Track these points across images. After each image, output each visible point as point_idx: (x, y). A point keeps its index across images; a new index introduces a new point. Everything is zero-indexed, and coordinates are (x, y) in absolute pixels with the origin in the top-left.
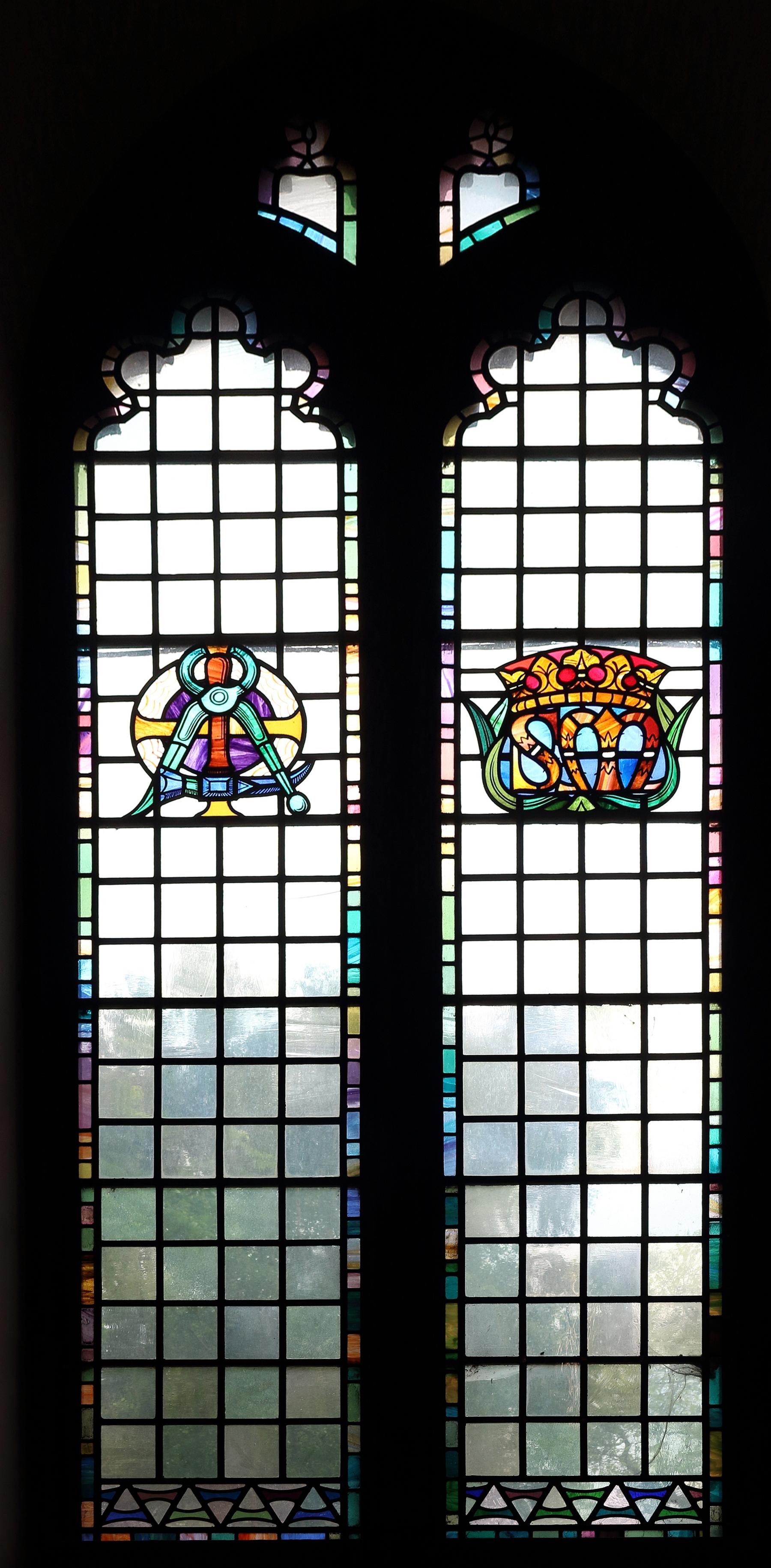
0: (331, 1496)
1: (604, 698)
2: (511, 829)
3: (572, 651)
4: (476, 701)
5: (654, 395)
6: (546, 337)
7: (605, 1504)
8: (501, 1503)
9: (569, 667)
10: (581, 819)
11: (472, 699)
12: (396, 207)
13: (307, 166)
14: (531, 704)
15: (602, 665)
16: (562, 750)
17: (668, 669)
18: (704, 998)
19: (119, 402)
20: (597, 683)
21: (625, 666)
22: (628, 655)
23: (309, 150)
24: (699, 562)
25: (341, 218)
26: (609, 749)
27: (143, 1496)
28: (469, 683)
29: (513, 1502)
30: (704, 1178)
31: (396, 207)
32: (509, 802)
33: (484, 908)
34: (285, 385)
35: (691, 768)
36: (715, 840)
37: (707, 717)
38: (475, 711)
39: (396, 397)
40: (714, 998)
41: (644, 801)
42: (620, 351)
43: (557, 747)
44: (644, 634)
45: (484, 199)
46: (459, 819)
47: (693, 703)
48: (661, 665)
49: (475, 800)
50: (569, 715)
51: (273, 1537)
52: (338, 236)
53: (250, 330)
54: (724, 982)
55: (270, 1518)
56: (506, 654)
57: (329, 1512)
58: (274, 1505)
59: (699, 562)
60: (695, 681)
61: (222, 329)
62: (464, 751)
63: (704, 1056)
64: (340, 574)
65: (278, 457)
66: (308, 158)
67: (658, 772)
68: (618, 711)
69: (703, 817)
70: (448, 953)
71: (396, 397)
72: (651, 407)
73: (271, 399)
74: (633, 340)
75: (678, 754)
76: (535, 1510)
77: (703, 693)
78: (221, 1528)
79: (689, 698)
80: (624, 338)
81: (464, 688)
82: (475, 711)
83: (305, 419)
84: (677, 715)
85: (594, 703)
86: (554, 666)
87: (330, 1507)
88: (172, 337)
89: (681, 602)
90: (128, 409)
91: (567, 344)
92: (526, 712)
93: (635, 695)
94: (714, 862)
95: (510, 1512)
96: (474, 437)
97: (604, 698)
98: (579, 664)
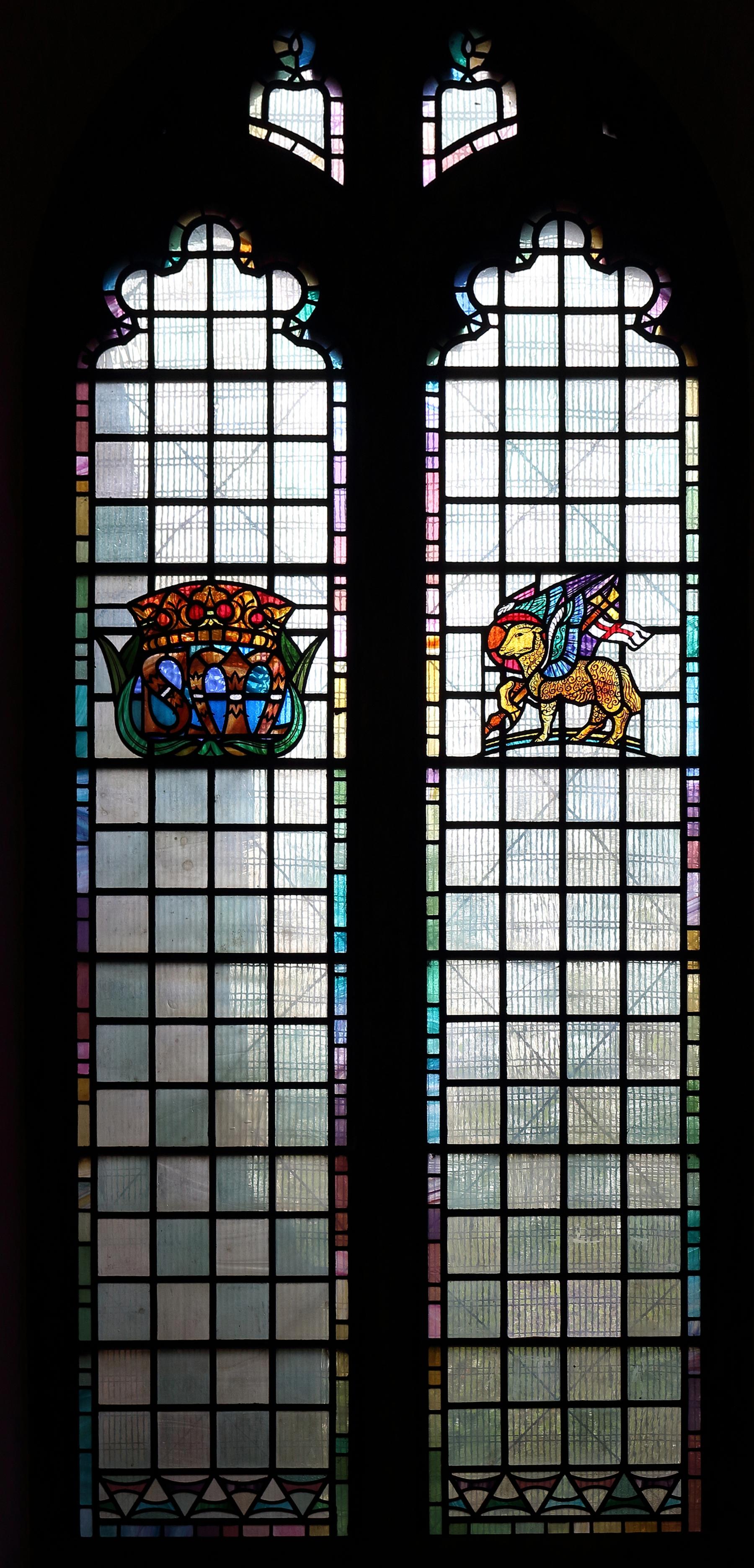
2: (140, 779)
4: (111, 638)
6: (527, 256)
8: (648, 1494)
9: (199, 603)
11: (109, 637)
12: (383, 126)
13: (297, 80)
17: (295, 607)
18: (680, 956)
19: (468, 320)
21: (252, 601)
22: (254, 589)
23: (297, 63)
28: (103, 619)
30: (329, 1152)
31: (383, 126)
32: (143, 747)
33: (468, 857)
35: (317, 711)
36: (341, 788)
37: (332, 659)
38: (108, 648)
39: (385, 310)
40: (693, 955)
41: (271, 747)
44: (271, 569)
45: (468, 114)
47: (316, 645)
48: (288, 603)
49: (109, 743)
51: (299, 1531)
54: (349, 943)
55: (290, 1508)
56: (138, 587)
57: (461, 1502)
58: (295, 1497)
60: (318, 619)
62: (97, 690)
63: (329, 1021)
65: (270, 375)
66: (296, 72)
69: (328, 764)
71: (385, 310)
75: (306, 697)
76: (136, 1504)
77: (327, 634)
78: (535, 1517)
79: (313, 638)
80: (251, 265)
82: (108, 648)
83: (299, 342)
87: (111, 1494)
88: (520, 252)
90: (478, 327)
91: (546, 265)
94: (692, 812)
95: (229, 1505)
96: (456, 358)
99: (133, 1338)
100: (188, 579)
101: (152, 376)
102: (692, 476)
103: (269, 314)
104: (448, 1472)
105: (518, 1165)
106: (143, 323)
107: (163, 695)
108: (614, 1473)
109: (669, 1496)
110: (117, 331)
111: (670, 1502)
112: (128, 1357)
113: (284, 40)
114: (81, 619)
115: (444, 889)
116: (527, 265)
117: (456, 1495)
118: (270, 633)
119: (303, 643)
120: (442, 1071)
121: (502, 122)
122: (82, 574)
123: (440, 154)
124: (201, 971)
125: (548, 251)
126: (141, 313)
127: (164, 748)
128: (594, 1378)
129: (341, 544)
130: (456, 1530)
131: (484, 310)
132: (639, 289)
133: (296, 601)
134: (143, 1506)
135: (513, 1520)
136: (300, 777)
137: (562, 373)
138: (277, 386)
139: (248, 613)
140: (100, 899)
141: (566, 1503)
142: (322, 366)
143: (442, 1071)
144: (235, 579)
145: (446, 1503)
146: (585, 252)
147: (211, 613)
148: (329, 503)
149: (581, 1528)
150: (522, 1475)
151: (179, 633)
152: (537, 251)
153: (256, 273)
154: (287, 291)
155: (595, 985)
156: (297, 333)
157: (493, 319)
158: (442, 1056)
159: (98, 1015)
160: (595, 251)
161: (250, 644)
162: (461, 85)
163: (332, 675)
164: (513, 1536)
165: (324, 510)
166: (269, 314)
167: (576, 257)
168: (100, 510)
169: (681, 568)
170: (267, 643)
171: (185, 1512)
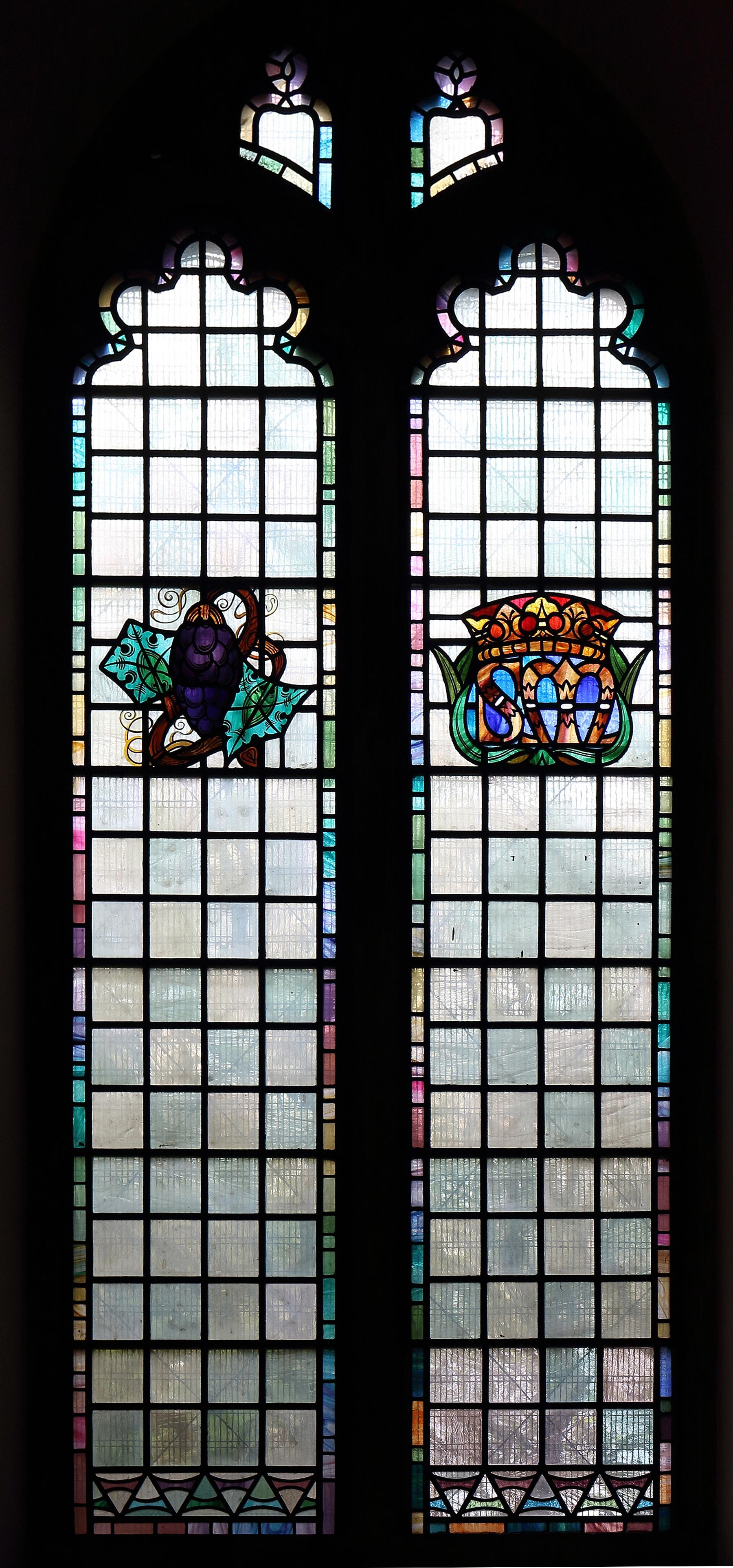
0: (104, 1504)
1: (562, 647)
3: (533, 598)
4: (445, 648)
5: (269, 340)
6: (506, 278)
7: (186, 1494)
9: (531, 614)
10: (543, 773)
11: (464, 647)
12: (373, 148)
14: (495, 652)
15: (560, 614)
16: (525, 702)
20: (555, 632)
22: (584, 602)
24: (649, 511)
25: (317, 160)
26: (567, 701)
27: (277, 1485)
28: (438, 630)
29: (280, 1493)
31: (373, 148)
34: (603, 325)
35: (643, 721)
37: (657, 672)
38: (443, 659)
42: (575, 295)
43: (519, 698)
44: (599, 583)
45: (456, 142)
46: (428, 771)
47: (644, 654)
48: (615, 615)
49: (444, 752)
50: (531, 665)
52: (314, 178)
53: (571, 268)
56: (471, 599)
59: (649, 511)
60: (644, 632)
61: (545, 267)
62: (432, 699)
64: (91, 516)
65: (262, 393)
66: (286, 96)
67: (612, 727)
68: (576, 661)
70: (417, 914)
72: (602, 353)
73: (254, 338)
74: (587, 282)
75: (632, 708)
77: (652, 646)
80: (578, 284)
81: (434, 634)
84: (629, 666)
85: (554, 653)
86: (516, 613)
87: (105, 1492)
88: (499, 274)
89: (632, 551)
90: (459, 348)
91: (525, 286)
92: (493, 659)
93: (590, 645)
95: (220, 1503)
96: (104, 376)
97: (562, 647)
98: (539, 612)
99: (449, 1337)
100: (517, 592)
101: (483, 393)
102: (330, 495)
103: (260, 330)
104: (92, 1472)
105: (498, 1169)
106: (474, 340)
107: (497, 704)
108: (253, 1474)
109: (304, 1498)
110: (442, 350)
111: (306, 1504)
112: (241, 1356)
113: (277, 63)
114: (416, 631)
115: (91, 897)
116: (507, 287)
117: (437, 1495)
118: (598, 643)
119: (631, 654)
120: (87, 1077)
121: (490, 150)
122: (79, 585)
123: (430, 181)
124: (253, 975)
125: (527, 274)
126: (136, 329)
127: (496, 756)
128: (234, 1379)
129: (329, 559)
130: (102, 1529)
131: (465, 332)
132: (613, 311)
133: (626, 613)
134: (135, 1504)
135: (211, 1520)
136: (636, 787)
137: (204, 393)
138: (153, 402)
139: (578, 623)
140: (95, 904)
141: (264, 1504)
142: (647, 385)
143: (87, 1077)
144: (568, 592)
145: (91, 1504)
146: (562, 274)
147: (543, 624)
148: (317, 519)
149: (218, 1529)
150: (557, 1474)
151: (513, 643)
152: (516, 273)
153: (247, 291)
154: (277, 307)
155: (570, 994)
156: (622, 351)
157: (138, 338)
158: (88, 1063)
159: (95, 1019)
160: (236, 272)
161: (579, 656)
162: (278, 109)
163: (656, 687)
164: (155, 1537)
165: (313, 526)
166: (260, 330)
167: (552, 279)
168: (95, 523)
169: (318, 583)
170: (595, 653)
171: (177, 1509)
